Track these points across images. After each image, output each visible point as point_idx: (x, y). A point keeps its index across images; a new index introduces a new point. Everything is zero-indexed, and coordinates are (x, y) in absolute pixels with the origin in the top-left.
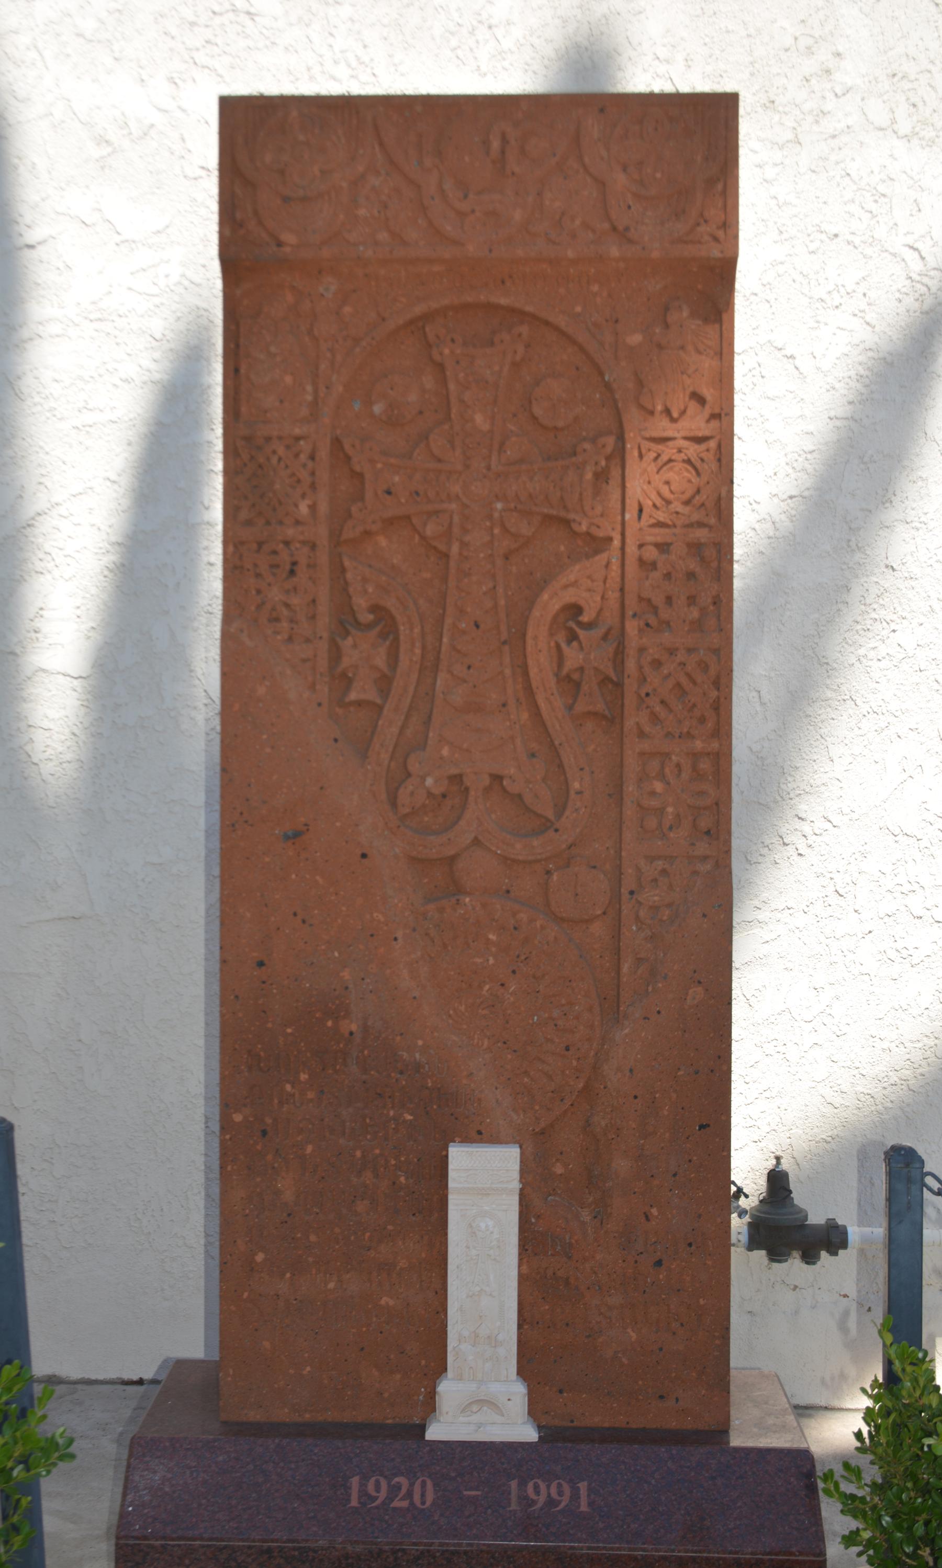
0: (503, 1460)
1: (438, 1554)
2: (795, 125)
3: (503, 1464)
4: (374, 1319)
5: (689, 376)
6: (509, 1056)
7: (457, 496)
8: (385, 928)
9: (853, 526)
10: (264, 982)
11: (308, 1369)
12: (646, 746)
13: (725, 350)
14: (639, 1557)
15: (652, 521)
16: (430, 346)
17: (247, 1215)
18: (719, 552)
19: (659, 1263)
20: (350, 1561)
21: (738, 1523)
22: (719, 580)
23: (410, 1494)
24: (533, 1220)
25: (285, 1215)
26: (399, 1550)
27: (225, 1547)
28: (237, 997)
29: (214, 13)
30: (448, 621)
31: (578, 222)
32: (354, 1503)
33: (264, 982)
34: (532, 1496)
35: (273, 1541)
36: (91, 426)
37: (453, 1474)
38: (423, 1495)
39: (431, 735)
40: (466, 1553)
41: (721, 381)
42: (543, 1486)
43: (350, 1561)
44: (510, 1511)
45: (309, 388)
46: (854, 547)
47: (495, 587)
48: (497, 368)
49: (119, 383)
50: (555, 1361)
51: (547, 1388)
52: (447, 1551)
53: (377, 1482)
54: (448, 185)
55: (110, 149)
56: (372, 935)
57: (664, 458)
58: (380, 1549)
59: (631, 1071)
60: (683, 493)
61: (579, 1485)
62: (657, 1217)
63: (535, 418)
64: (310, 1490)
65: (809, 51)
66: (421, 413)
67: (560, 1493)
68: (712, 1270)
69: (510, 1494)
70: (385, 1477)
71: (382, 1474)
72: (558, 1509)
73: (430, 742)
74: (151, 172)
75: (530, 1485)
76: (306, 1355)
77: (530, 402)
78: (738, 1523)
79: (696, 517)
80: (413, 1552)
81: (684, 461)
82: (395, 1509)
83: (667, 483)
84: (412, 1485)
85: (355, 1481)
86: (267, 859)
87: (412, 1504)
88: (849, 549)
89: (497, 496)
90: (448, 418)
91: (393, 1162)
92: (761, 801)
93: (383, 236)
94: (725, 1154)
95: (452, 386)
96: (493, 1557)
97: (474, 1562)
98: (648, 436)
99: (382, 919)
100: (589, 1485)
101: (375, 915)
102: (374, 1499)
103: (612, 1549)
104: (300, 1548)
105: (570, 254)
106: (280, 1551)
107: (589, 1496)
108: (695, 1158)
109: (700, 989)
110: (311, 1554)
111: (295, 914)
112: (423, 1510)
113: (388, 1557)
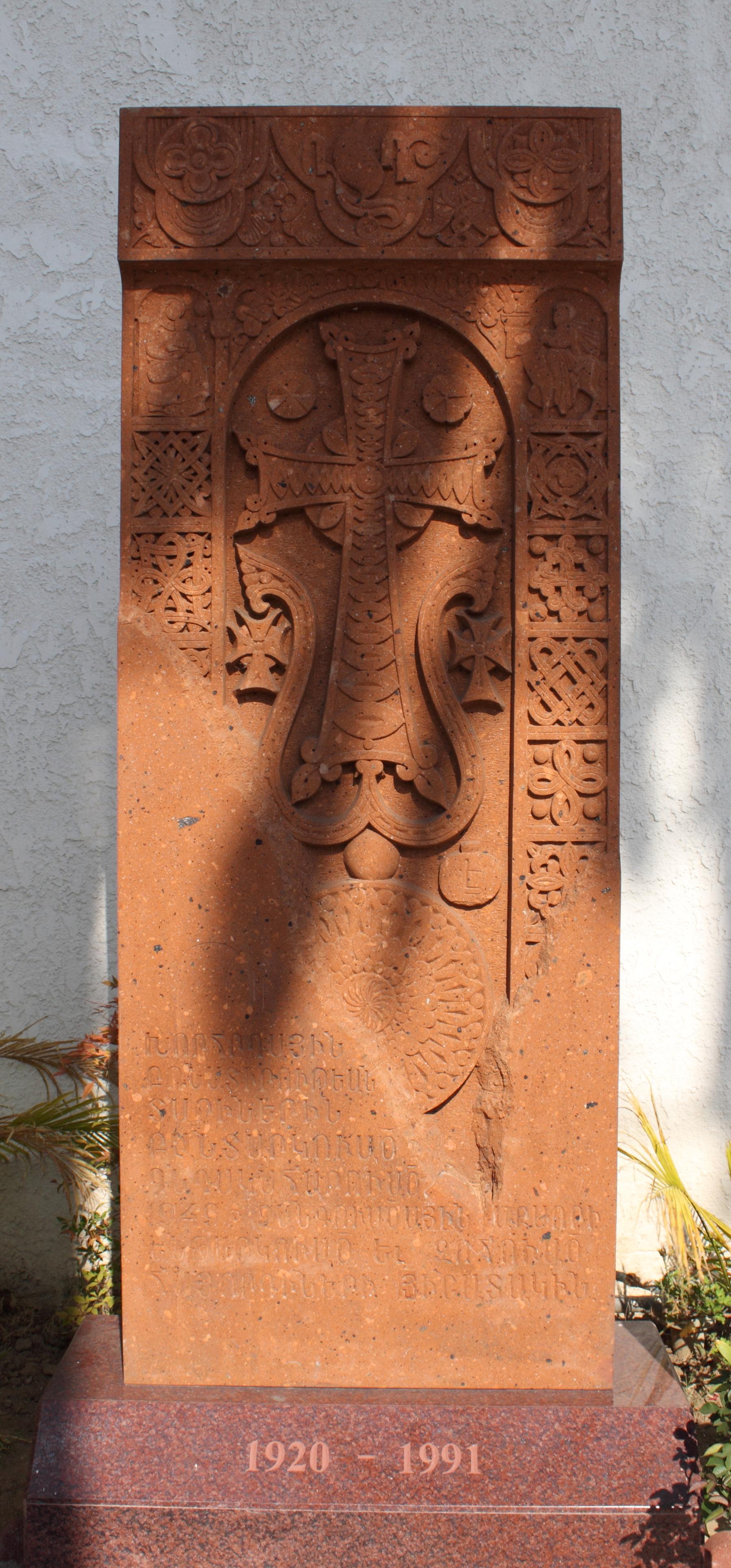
0: (396, 1425)
1: (333, 1517)
2: (658, 174)
3: (396, 1428)
4: (272, 1290)
5: (577, 375)
6: (403, 1038)
7: (351, 488)
8: (280, 913)
9: (716, 530)
10: (161, 966)
11: (209, 1336)
12: (537, 733)
13: (610, 350)
14: (527, 1517)
15: (541, 514)
16: (323, 344)
17: (147, 1192)
18: (606, 544)
19: (547, 1236)
20: (249, 1523)
21: (622, 1482)
22: (607, 571)
23: (306, 1459)
24: (426, 1196)
25: (184, 1191)
26: (296, 1513)
27: (128, 1510)
28: (135, 980)
29: (135, 72)
30: (341, 611)
31: (467, 226)
32: (252, 1467)
33: (161, 966)
34: (424, 1458)
35: (173, 1505)
36: (18, 438)
37: (348, 1439)
38: (319, 1459)
39: (325, 722)
40: (360, 1515)
41: (607, 379)
42: (434, 1449)
43: (249, 1523)
44: (403, 1475)
45: (206, 384)
46: (717, 550)
47: (387, 577)
48: (389, 365)
49: (44, 399)
50: (447, 1329)
51: (439, 1353)
52: (342, 1513)
53: (275, 1447)
54: (340, 190)
55: (39, 192)
56: (267, 920)
57: (554, 452)
58: (278, 1512)
59: (521, 1051)
60: (571, 487)
61: (469, 1448)
62: (546, 1192)
63: (427, 414)
64: (210, 1454)
65: (670, 112)
66: (315, 408)
67: (452, 1457)
68: (598, 1241)
69: (403, 1458)
70: (283, 1442)
71: (279, 1439)
72: (449, 1472)
73: (323, 729)
74: (76, 211)
75: (423, 1449)
76: (207, 1324)
77: (422, 398)
78: (622, 1482)
79: (584, 510)
80: (310, 1514)
81: (572, 456)
82: (291, 1473)
83: (557, 477)
84: (308, 1449)
85: (253, 1446)
86: (164, 846)
87: (308, 1468)
88: (713, 552)
89: (389, 488)
90: (342, 412)
91: (289, 1141)
92: (634, 782)
93: (278, 238)
94: (612, 1130)
95: (345, 383)
96: (386, 1519)
97: (368, 1523)
98: (537, 431)
99: (277, 905)
100: (480, 1448)
101: (270, 900)
102: (271, 1463)
103: (502, 1510)
104: (200, 1511)
105: (460, 256)
106: (181, 1514)
107: (479, 1458)
108: (583, 1135)
109: (589, 972)
110: (210, 1516)
111: (191, 900)
112: (319, 1474)
113: (285, 1519)
